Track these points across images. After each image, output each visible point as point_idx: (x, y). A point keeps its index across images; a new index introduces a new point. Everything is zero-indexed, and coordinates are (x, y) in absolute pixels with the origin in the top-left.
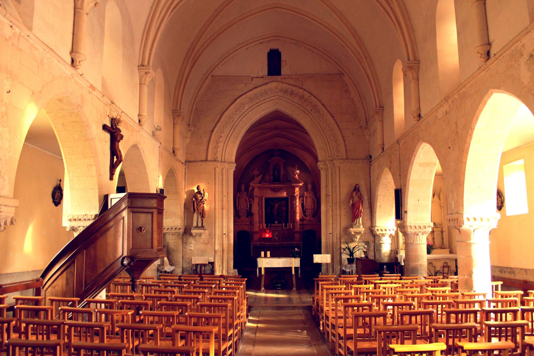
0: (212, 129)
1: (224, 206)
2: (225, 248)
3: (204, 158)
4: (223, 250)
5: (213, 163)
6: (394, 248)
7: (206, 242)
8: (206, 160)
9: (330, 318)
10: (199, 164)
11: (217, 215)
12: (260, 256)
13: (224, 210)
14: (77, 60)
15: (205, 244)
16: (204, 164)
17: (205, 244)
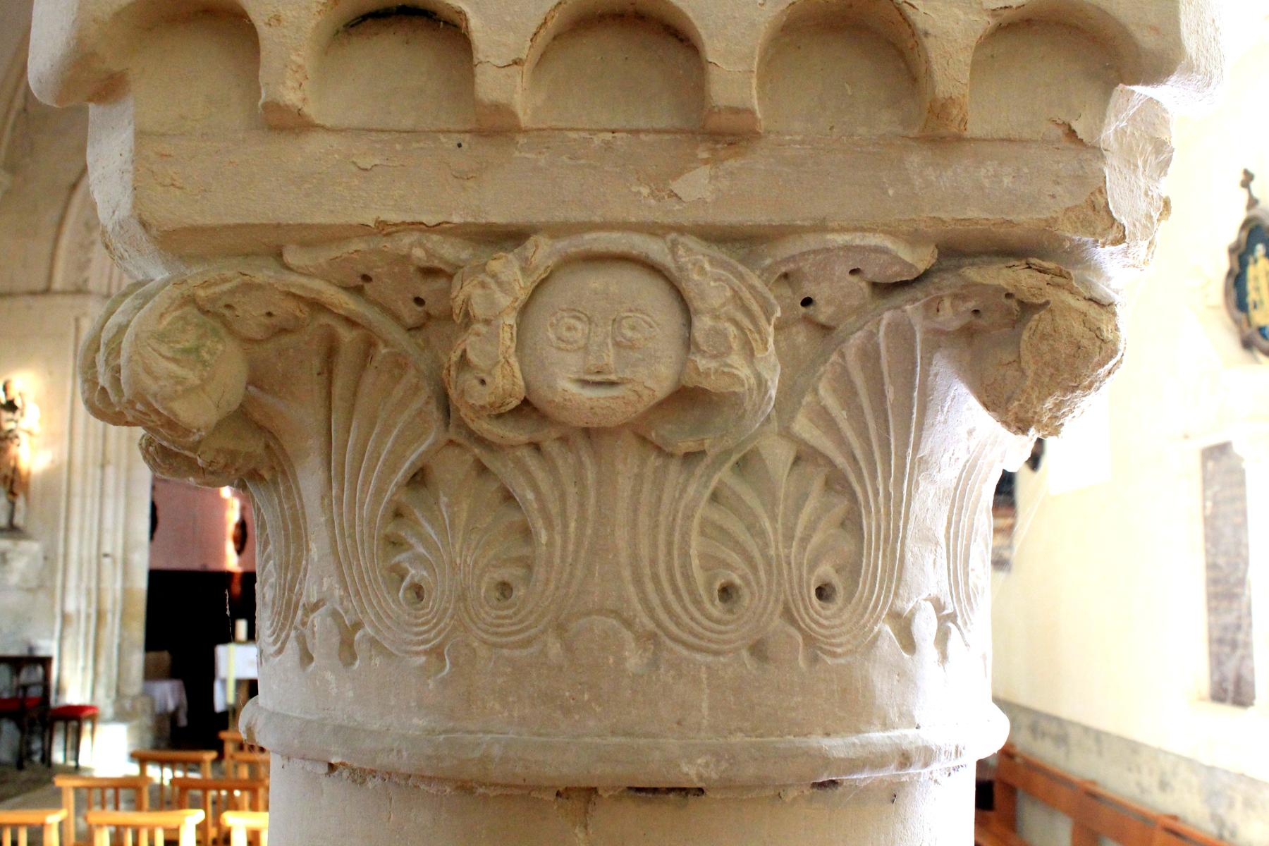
0: (72, 179)
1: (111, 456)
2: (108, 604)
3: (41, 285)
4: (100, 615)
5: (68, 301)
6: (1216, 678)
7: (33, 584)
8: (47, 291)
9: (929, 769)
10: (21, 302)
11: (77, 488)
12: (229, 637)
13: (110, 470)
14: (1014, 555)
15: (29, 590)
16: (40, 303)
17: (29, 590)
